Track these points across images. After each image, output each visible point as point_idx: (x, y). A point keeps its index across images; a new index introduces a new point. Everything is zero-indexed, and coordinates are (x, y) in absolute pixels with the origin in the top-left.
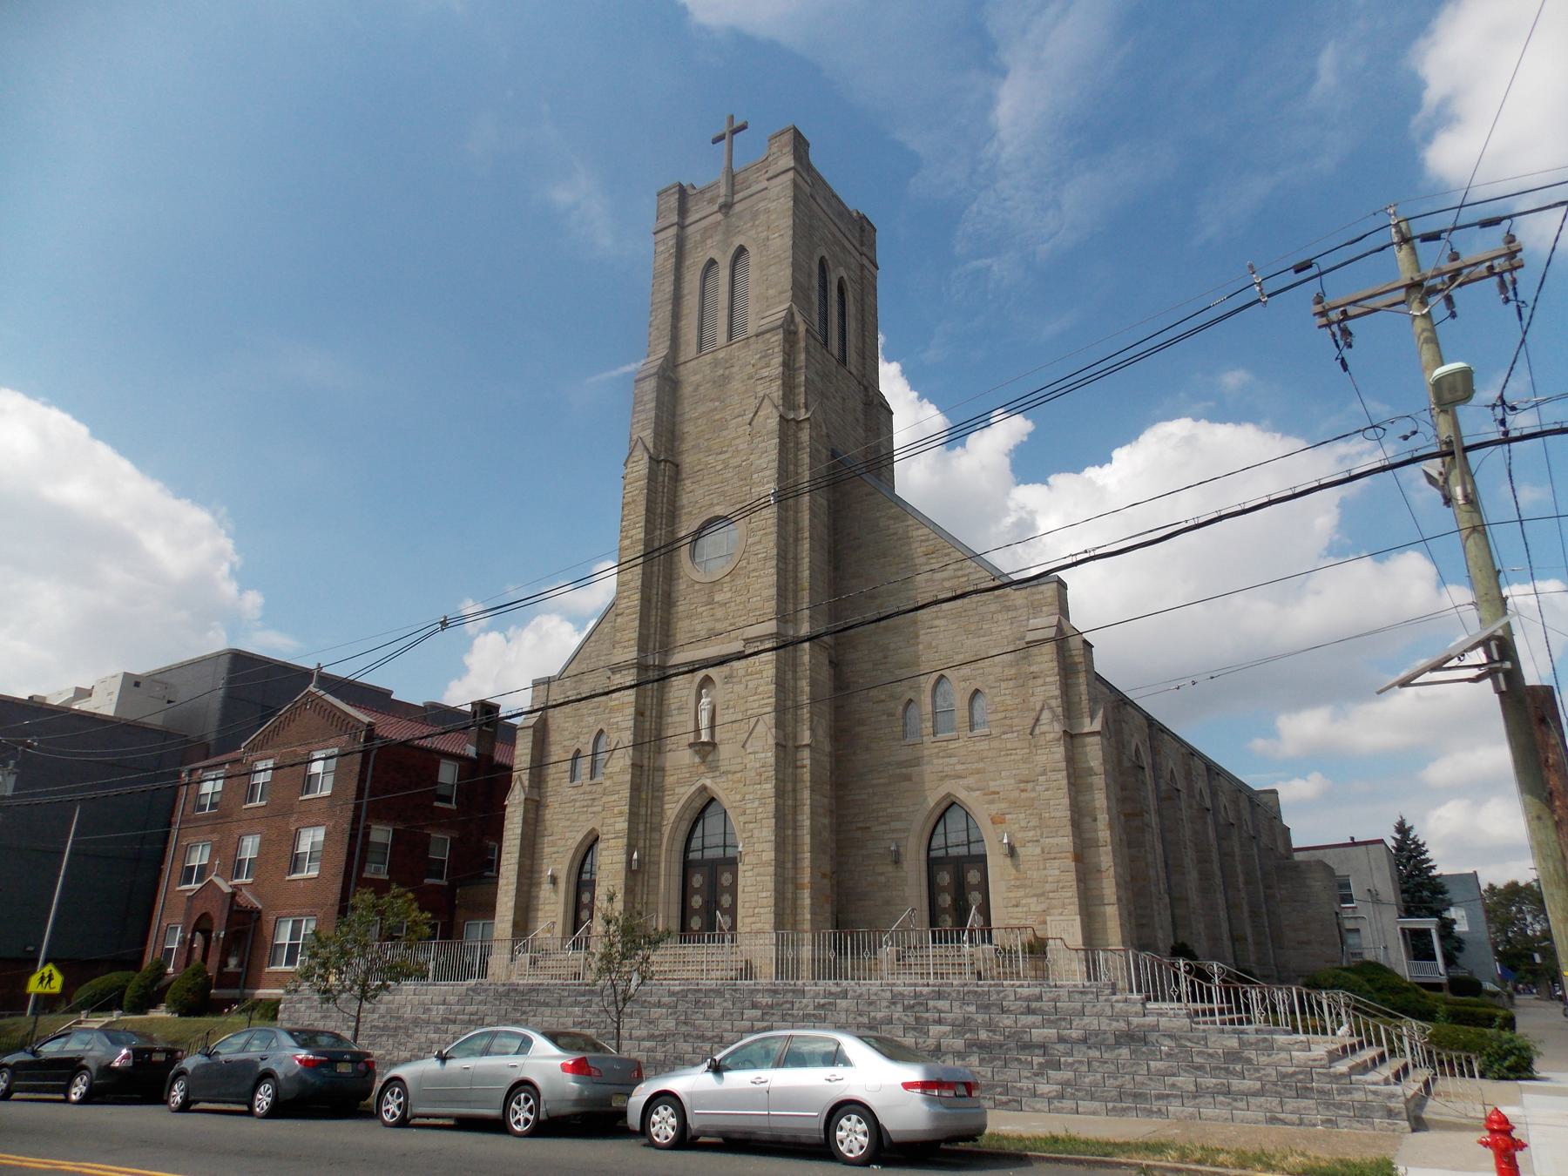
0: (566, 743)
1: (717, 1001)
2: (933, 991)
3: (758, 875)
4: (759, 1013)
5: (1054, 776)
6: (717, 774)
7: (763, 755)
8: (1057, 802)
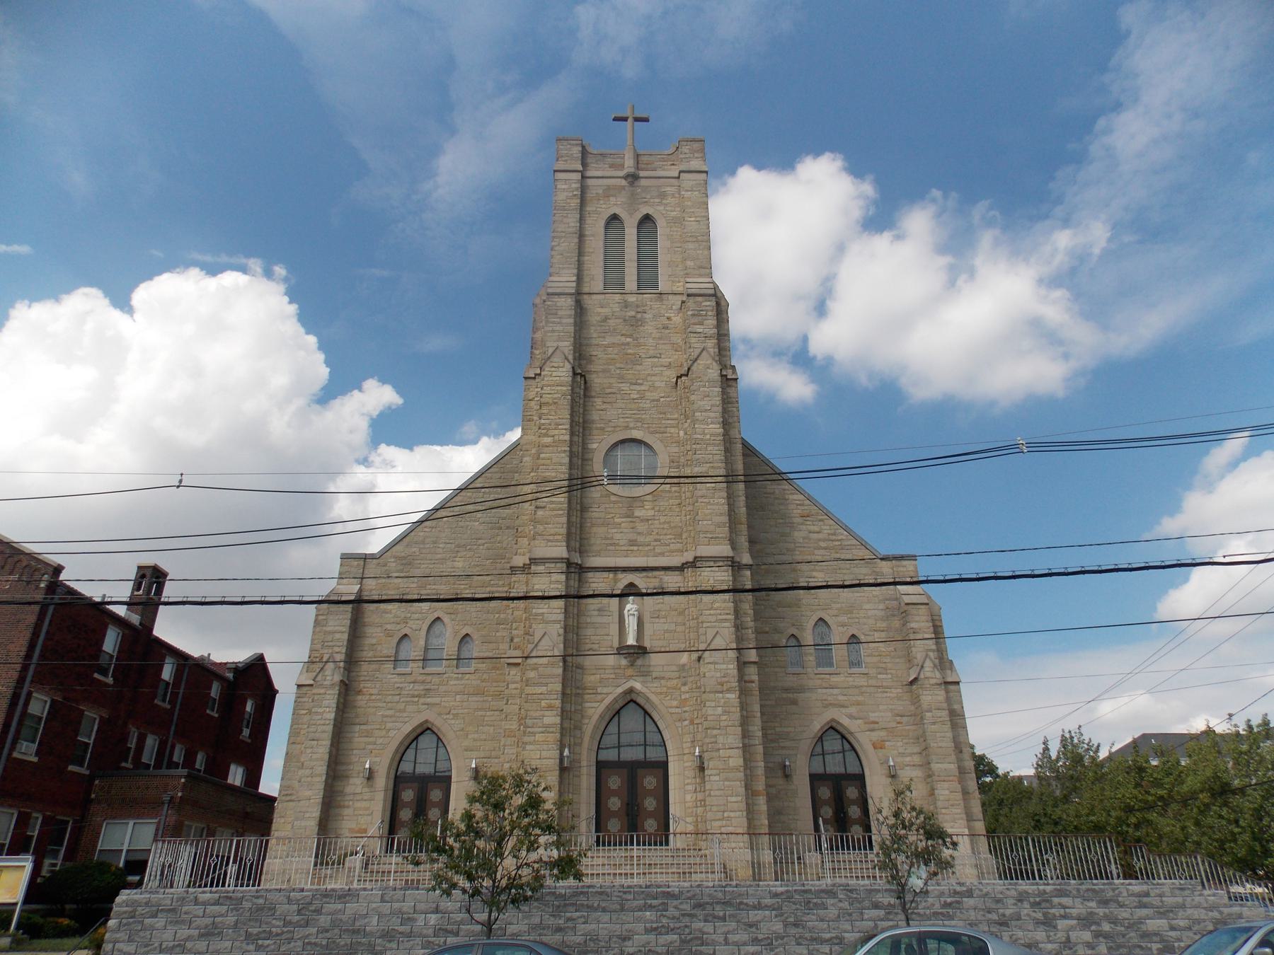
0: (389, 627)
1: (830, 901)
2: (1055, 889)
3: (727, 780)
4: (882, 913)
5: (939, 713)
6: (649, 678)
8: (942, 734)
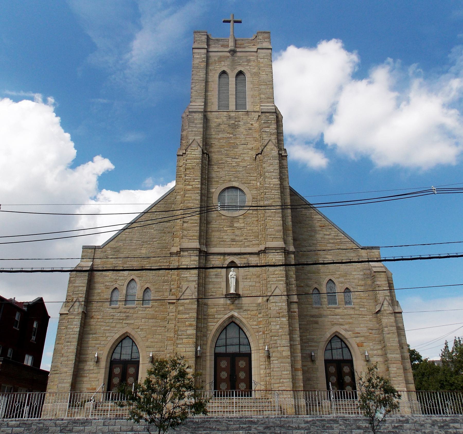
0: (107, 284)
1: (335, 425)
6: (242, 310)
7: (280, 304)
